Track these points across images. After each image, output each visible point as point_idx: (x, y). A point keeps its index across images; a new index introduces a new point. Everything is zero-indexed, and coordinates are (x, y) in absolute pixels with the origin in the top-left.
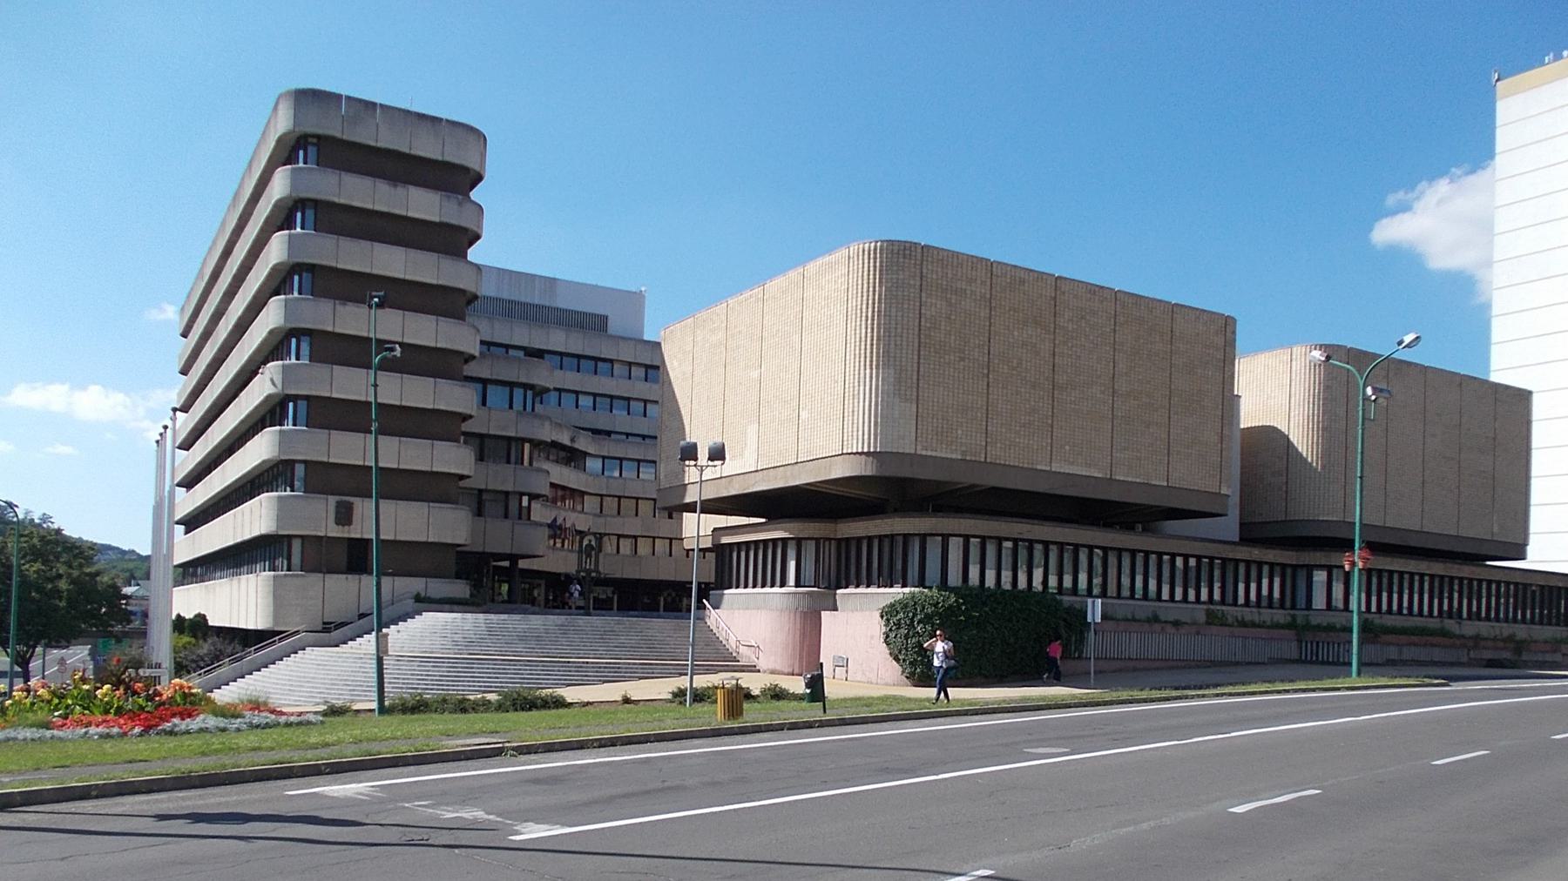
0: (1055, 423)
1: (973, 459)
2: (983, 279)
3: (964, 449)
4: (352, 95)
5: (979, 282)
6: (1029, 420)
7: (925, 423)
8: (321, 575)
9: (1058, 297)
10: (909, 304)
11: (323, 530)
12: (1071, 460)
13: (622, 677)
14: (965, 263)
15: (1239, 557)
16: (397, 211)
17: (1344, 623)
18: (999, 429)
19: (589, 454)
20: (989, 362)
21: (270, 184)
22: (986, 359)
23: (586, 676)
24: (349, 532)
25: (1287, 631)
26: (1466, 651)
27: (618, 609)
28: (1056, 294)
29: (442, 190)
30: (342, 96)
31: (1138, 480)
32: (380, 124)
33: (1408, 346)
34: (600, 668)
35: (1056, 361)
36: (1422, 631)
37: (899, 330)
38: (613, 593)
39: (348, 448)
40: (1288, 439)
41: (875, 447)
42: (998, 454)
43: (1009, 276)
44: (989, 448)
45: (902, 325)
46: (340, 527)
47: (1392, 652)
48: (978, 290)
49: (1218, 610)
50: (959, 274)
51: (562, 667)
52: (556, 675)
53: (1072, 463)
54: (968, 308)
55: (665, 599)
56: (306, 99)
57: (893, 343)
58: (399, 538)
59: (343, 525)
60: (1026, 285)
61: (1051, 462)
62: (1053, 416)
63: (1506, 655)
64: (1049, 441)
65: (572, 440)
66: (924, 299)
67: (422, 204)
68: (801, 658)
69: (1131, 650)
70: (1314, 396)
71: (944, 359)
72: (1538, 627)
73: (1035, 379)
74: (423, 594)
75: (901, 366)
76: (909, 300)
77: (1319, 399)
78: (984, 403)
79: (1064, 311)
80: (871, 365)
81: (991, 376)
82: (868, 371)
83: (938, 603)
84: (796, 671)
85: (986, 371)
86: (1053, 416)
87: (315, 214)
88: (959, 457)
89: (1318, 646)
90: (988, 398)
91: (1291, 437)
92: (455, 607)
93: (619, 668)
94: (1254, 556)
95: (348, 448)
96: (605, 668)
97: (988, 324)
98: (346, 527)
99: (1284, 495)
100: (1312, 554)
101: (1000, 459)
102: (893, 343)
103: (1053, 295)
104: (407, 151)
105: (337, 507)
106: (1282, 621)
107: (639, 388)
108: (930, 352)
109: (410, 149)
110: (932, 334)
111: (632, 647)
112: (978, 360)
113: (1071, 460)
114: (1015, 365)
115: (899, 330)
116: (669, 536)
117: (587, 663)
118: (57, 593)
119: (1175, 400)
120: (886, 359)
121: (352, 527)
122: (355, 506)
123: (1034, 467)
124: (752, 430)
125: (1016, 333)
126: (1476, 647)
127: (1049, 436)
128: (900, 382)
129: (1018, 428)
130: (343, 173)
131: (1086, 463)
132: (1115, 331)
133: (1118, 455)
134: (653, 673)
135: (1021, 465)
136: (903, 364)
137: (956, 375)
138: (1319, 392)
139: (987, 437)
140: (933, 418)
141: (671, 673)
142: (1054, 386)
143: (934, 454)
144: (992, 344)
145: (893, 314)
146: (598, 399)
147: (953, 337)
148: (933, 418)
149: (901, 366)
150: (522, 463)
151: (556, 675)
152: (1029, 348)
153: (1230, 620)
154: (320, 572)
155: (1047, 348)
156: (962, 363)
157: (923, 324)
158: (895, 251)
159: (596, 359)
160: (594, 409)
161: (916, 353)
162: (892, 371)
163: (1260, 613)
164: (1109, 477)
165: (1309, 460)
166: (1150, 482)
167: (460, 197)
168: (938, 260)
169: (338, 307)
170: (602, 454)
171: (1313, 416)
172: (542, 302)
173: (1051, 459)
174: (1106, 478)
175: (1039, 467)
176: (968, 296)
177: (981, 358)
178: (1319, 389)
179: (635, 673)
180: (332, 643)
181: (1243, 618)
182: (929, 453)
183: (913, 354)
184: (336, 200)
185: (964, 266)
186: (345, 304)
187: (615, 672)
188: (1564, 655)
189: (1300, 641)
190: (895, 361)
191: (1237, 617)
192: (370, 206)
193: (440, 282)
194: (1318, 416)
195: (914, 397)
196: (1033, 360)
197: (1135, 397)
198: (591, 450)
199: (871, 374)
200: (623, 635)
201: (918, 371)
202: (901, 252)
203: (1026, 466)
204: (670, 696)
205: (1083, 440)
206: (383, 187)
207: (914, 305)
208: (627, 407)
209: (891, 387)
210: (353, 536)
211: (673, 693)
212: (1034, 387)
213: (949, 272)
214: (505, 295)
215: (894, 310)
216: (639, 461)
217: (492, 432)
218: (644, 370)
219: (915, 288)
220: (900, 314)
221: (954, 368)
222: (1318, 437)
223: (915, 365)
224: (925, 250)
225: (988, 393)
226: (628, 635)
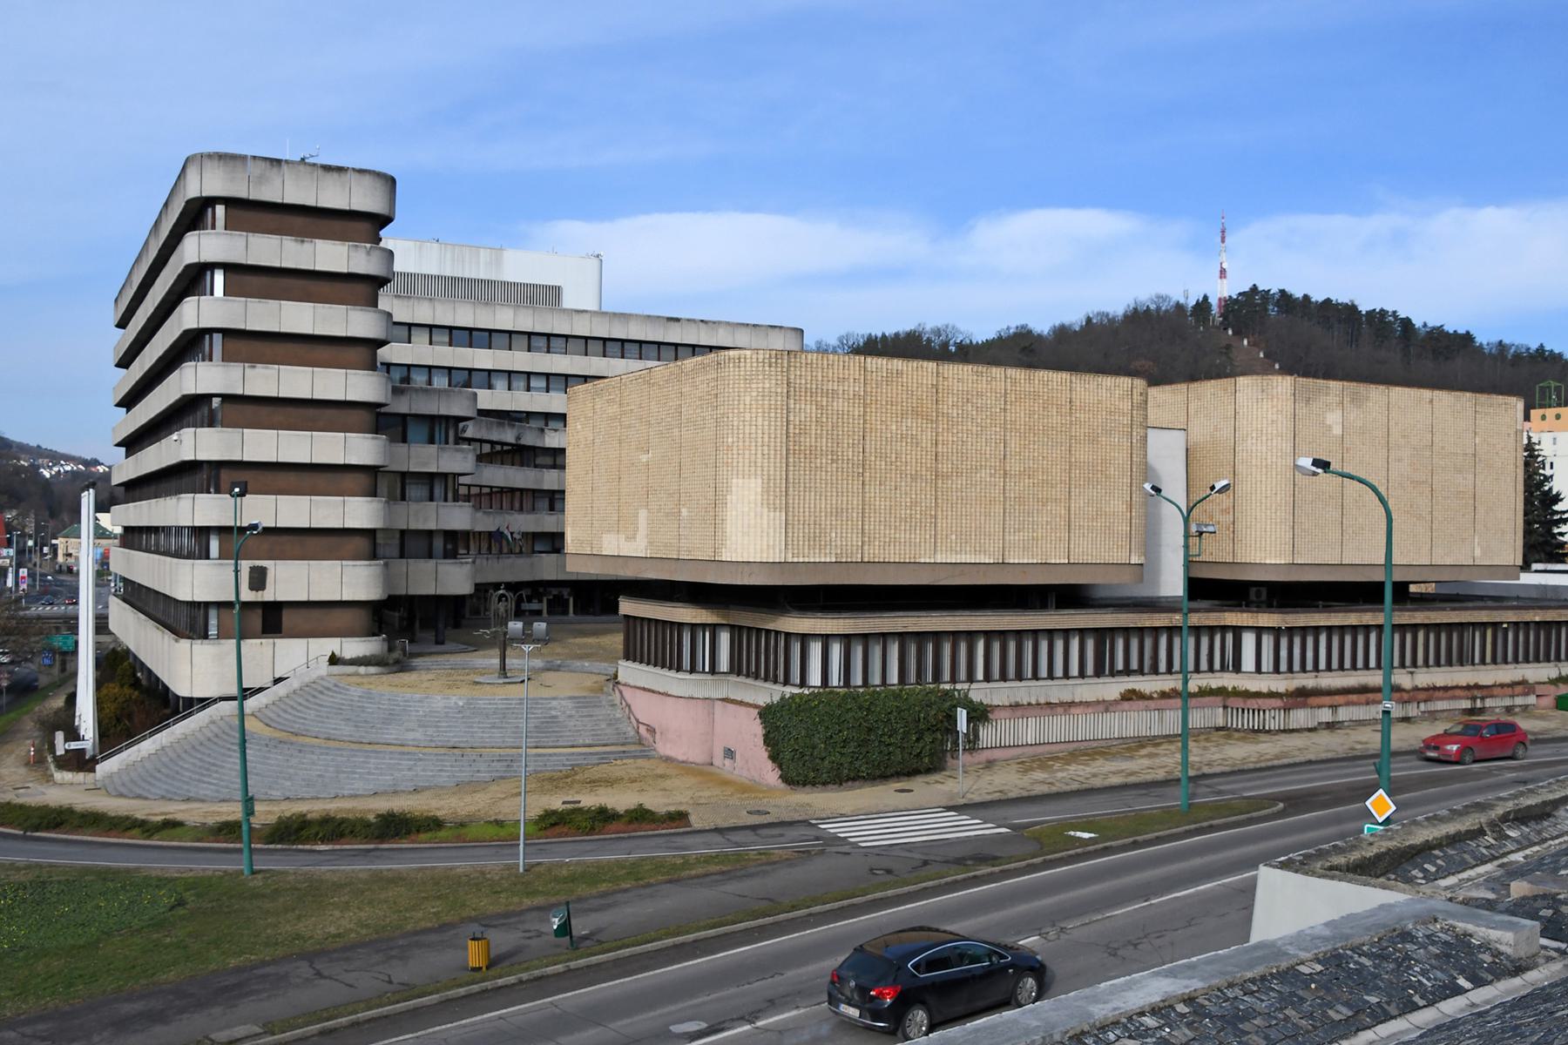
15: (1157, 624)
21: (180, 247)
26: (1416, 705)
33: (1220, 491)
38: (569, 595)
42: (873, 553)
57: (759, 452)
59: (257, 591)
74: (337, 653)
99: (1232, 535)
100: (1239, 614)
115: (766, 440)
119: (1076, 473)
122: (268, 572)
124: (643, 514)
128: (768, 492)
130: (250, 234)
142: (936, 476)
158: (760, 360)
159: (549, 336)
161: (784, 461)
162: (760, 481)
185: (836, 367)
189: (1225, 707)
202: (766, 361)
206: (289, 243)
209: (759, 497)
215: (760, 419)
223: (784, 473)
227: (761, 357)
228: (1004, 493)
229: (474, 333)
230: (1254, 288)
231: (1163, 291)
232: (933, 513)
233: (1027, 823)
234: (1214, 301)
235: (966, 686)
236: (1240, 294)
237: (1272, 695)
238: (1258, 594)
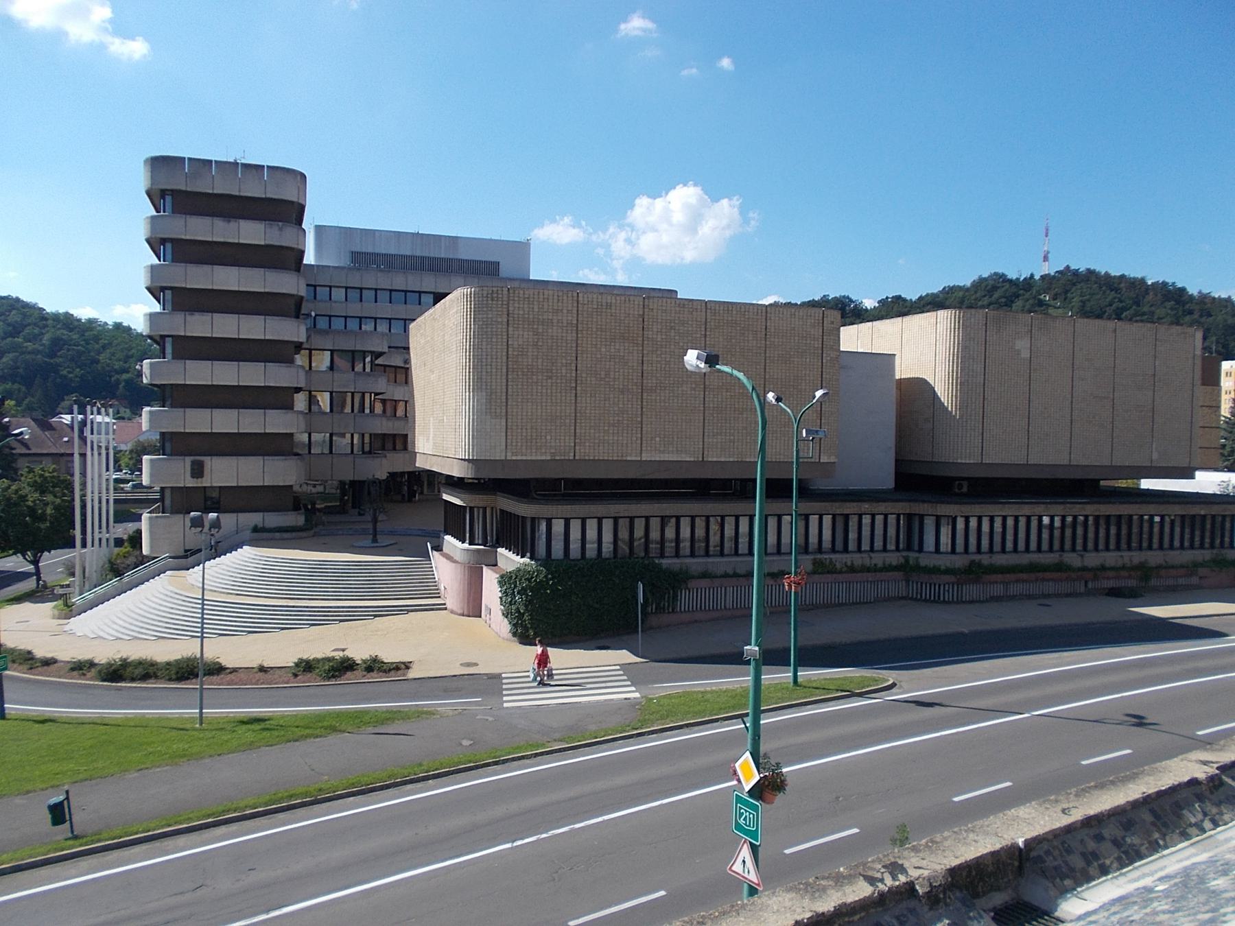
0: (644, 419)
1: (563, 458)
2: (570, 309)
3: (553, 451)
4: (193, 157)
5: (565, 311)
6: (618, 420)
7: (514, 434)
8: (182, 516)
9: (646, 313)
10: (497, 338)
11: (183, 482)
12: (662, 449)
14: (551, 297)
17: (948, 565)
18: (588, 431)
20: (576, 377)
22: (574, 375)
24: (202, 483)
25: (896, 573)
28: (644, 312)
30: (185, 158)
31: (731, 460)
35: (645, 368)
36: (1033, 568)
37: (489, 360)
39: (199, 421)
40: (934, 391)
41: (473, 456)
43: (595, 303)
44: (577, 448)
45: (492, 355)
46: (195, 479)
47: (998, 590)
48: (565, 318)
49: (826, 559)
50: (546, 307)
53: (663, 452)
54: (555, 334)
56: (159, 164)
57: (484, 370)
59: (197, 478)
60: (613, 308)
61: (641, 453)
62: (642, 415)
63: (1132, 583)
64: (639, 435)
66: (510, 332)
67: (251, 233)
68: (468, 602)
69: (728, 601)
70: (954, 355)
71: (532, 379)
72: (1178, 552)
73: (623, 385)
75: (491, 389)
76: (497, 335)
77: (958, 358)
78: (573, 411)
79: (653, 325)
80: (469, 389)
81: (578, 388)
82: (467, 394)
83: (532, 578)
84: (466, 613)
85: (574, 385)
86: (642, 415)
88: (549, 458)
89: (922, 586)
90: (576, 406)
91: (936, 389)
94: (863, 509)
95: (199, 421)
97: (574, 345)
101: (589, 456)
102: (484, 370)
103: (641, 313)
104: (237, 194)
106: (894, 563)
108: (517, 375)
109: (240, 191)
110: (520, 360)
112: (566, 376)
113: (662, 449)
114: (603, 376)
115: (489, 360)
118: (42, 518)
120: (479, 384)
123: (624, 459)
125: (603, 350)
126: (1096, 578)
127: (639, 432)
129: (606, 428)
130: (188, 216)
131: (677, 451)
132: (705, 335)
133: (710, 440)
135: (611, 458)
136: (494, 387)
137: (544, 391)
138: (958, 352)
139: (575, 439)
140: (522, 429)
142: (642, 389)
143: (524, 458)
144: (579, 362)
145: (484, 347)
147: (540, 361)
148: (522, 429)
149: (491, 389)
152: (617, 360)
153: (838, 566)
154: (181, 513)
155: (636, 358)
156: (549, 381)
157: (510, 353)
161: (504, 377)
162: (484, 394)
163: (871, 558)
164: (701, 459)
165: (950, 409)
166: (744, 460)
167: (280, 224)
168: (525, 298)
171: (953, 372)
172: (447, 256)
173: (641, 450)
174: (698, 461)
175: (629, 458)
176: (555, 324)
177: (568, 375)
178: (958, 349)
181: (852, 564)
182: (519, 458)
183: (501, 379)
184: (183, 237)
185: (551, 301)
188: (1201, 578)
190: (486, 385)
191: (846, 563)
192: (210, 239)
193: (267, 290)
194: (957, 373)
195: (504, 414)
196: (621, 371)
197: (727, 389)
199: (469, 396)
201: (507, 393)
203: (615, 458)
204: (293, 664)
205: (673, 432)
206: (219, 223)
207: (502, 338)
209: (484, 407)
210: (204, 485)
212: (622, 392)
213: (536, 307)
214: (418, 253)
215: (484, 343)
219: (502, 325)
220: (489, 346)
221: (542, 386)
222: (956, 390)
223: (504, 387)
224: (511, 291)
225: (576, 403)
227: (485, 293)
228: (704, 404)
229: (408, 294)
230: (1068, 267)
231: (1006, 273)
232: (639, 419)
233: (389, 711)
234: (1037, 277)
235: (917, 555)
236: (1057, 272)
237: (948, 571)
238: (960, 487)
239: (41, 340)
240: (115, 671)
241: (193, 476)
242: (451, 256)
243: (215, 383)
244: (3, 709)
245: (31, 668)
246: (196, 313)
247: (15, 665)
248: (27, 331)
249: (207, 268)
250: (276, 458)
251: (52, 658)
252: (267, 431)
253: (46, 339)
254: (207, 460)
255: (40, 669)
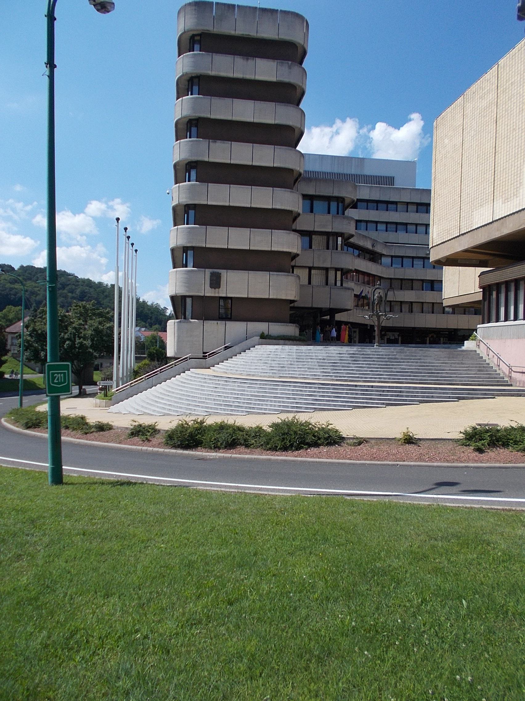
13: (404, 400)
16: (248, 77)
19: (384, 255)
23: (371, 399)
27: (401, 343)
29: (277, 59)
32: (237, 19)
34: (383, 391)
38: (399, 336)
46: (213, 289)
51: (350, 390)
52: (344, 397)
55: (429, 340)
58: (250, 296)
65: (373, 246)
87: (199, 88)
92: (287, 342)
93: (401, 392)
96: (388, 391)
98: (217, 290)
105: (211, 277)
107: (413, 217)
111: (412, 372)
116: (432, 302)
117: (372, 386)
121: (220, 289)
122: (222, 275)
134: (432, 397)
141: (449, 397)
146: (389, 226)
150: (337, 249)
151: (344, 397)
160: (387, 231)
167: (290, 62)
169: (211, 144)
170: (391, 254)
179: (415, 396)
180: (207, 367)
186: (216, 142)
187: (398, 396)
193: (277, 122)
198: (384, 252)
200: (403, 362)
204: (462, 436)
206: (239, 61)
208: (405, 229)
211: (466, 433)
216: (413, 258)
217: (316, 229)
218: (415, 207)
226: (408, 362)
239: (75, 292)
240: (191, 435)
241: (211, 287)
242: (359, 173)
243: (231, 204)
244: (62, 469)
245: (86, 433)
246: (218, 141)
247: (69, 431)
248: (69, 287)
249: (228, 101)
250: (280, 273)
251: (108, 424)
252: (273, 249)
253: (78, 291)
254: (223, 272)
255: (94, 433)
